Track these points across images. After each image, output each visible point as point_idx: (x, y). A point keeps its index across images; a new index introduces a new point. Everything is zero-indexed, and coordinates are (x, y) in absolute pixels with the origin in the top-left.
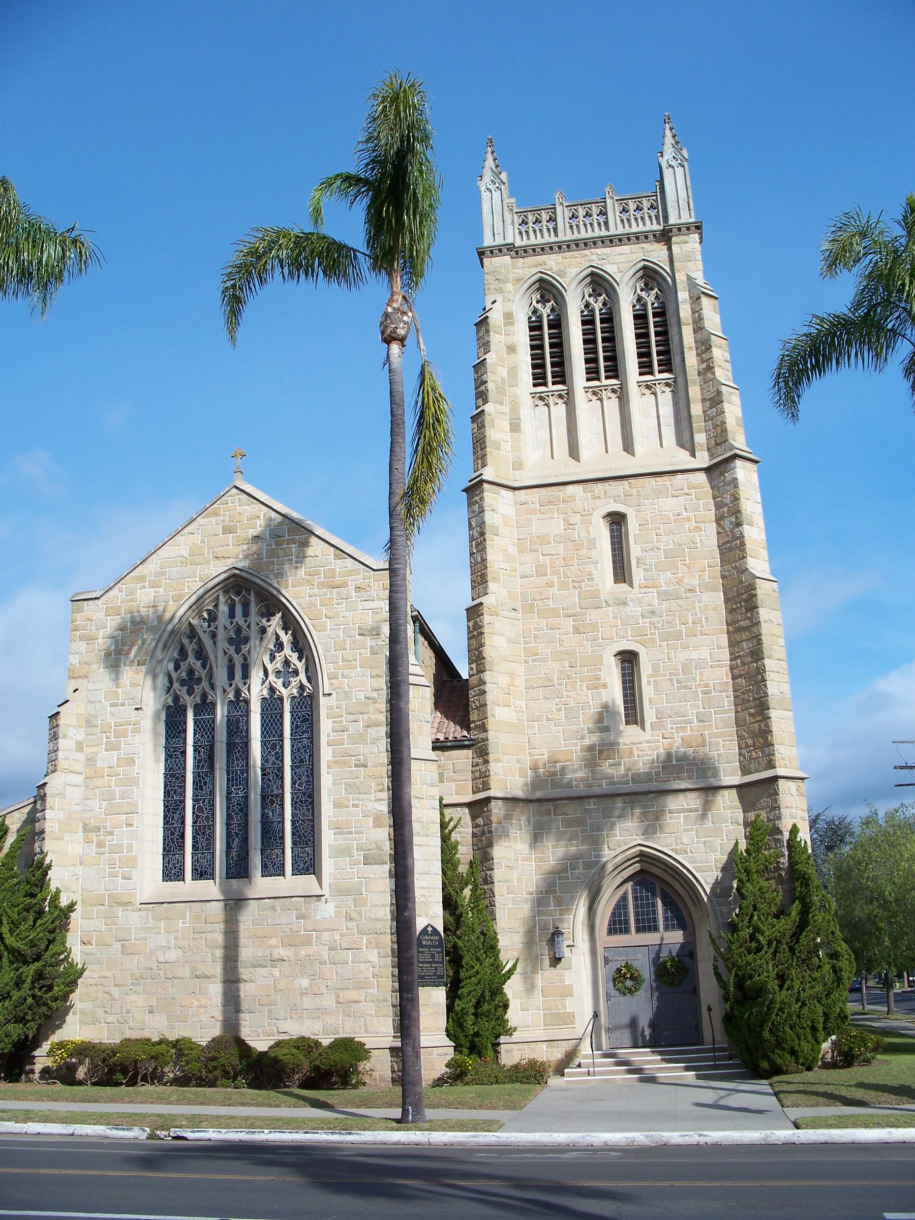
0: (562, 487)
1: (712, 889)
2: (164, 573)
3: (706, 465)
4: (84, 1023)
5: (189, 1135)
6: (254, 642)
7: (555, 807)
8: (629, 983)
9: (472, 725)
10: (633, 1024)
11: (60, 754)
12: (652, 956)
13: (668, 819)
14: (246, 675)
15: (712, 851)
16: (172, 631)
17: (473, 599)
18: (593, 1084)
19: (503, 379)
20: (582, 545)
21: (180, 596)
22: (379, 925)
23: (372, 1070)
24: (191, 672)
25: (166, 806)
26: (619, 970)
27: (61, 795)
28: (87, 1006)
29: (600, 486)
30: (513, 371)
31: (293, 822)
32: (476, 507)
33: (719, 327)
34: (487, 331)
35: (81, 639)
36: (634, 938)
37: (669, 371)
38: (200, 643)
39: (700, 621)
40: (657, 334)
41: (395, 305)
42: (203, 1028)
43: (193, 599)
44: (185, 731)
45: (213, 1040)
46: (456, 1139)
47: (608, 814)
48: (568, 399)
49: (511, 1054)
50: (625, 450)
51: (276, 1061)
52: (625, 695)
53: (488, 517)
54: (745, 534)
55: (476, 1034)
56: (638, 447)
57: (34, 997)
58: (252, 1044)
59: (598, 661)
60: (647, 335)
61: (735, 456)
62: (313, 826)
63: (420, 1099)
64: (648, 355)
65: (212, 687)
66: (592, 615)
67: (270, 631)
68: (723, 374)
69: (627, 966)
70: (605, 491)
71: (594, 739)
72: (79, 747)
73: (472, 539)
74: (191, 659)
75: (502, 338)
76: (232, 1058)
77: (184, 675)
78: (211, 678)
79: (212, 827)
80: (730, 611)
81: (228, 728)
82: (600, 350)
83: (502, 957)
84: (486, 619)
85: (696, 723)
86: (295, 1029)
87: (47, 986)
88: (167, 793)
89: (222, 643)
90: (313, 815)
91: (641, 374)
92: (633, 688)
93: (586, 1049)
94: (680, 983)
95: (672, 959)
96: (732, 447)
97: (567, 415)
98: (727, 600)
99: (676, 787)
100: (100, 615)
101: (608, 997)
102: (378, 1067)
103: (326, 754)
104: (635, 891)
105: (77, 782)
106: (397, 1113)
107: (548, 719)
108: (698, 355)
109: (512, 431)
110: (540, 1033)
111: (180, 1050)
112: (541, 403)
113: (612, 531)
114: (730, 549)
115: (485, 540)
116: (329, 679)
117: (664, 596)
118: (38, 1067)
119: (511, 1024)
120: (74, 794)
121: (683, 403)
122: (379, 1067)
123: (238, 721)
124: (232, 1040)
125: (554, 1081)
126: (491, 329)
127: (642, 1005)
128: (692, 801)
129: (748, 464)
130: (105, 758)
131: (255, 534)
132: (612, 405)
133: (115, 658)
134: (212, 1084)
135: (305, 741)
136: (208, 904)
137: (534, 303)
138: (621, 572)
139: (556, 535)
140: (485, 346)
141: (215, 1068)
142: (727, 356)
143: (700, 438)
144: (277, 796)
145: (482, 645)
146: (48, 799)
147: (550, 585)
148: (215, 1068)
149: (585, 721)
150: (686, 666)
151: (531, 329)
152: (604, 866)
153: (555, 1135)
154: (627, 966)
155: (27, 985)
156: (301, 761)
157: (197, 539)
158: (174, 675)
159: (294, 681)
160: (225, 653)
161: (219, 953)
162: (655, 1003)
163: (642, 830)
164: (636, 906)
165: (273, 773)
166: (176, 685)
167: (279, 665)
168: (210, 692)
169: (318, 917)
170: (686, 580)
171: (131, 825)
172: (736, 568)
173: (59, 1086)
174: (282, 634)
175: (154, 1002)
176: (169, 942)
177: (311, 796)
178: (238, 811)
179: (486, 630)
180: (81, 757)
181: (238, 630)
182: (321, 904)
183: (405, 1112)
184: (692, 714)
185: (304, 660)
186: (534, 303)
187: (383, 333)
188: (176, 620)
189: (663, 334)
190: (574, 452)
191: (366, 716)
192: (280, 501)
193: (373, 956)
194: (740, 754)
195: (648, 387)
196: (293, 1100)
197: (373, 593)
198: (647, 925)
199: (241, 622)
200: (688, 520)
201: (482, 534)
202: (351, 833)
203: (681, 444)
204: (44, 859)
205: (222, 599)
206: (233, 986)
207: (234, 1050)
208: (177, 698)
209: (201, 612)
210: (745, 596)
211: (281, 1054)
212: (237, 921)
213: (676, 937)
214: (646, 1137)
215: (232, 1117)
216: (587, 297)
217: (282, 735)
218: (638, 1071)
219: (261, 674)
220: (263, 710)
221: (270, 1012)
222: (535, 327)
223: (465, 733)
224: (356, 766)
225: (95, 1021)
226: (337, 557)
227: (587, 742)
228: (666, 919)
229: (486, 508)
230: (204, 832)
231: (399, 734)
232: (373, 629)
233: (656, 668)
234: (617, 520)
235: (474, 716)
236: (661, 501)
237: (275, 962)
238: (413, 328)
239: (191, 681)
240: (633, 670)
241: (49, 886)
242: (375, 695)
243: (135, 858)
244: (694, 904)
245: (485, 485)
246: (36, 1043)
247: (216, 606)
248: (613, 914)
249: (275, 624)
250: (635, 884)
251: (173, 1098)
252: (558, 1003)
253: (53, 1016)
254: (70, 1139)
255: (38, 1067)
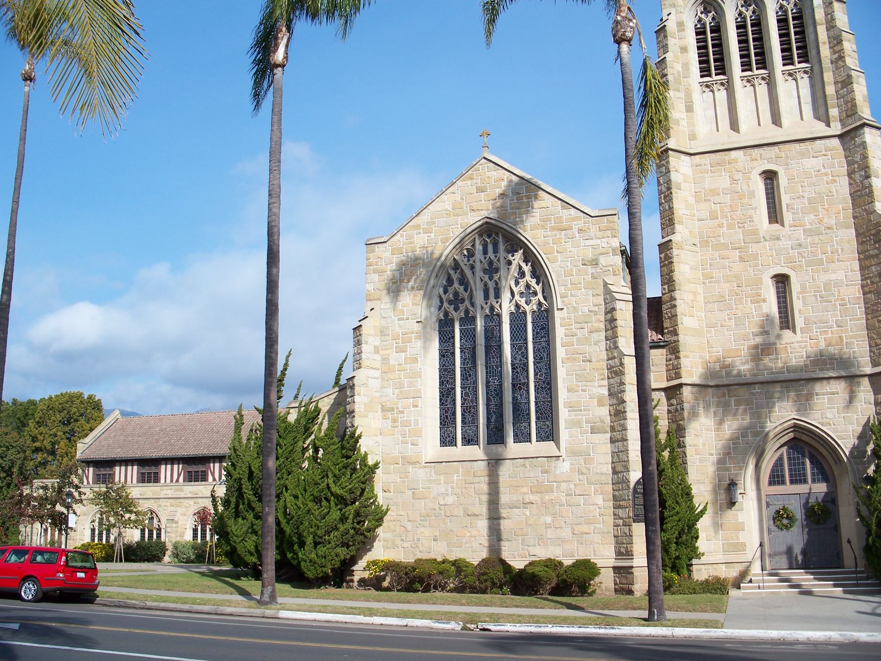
0: (727, 153)
1: (851, 452)
2: (434, 223)
3: (839, 133)
4: (387, 547)
5: (492, 627)
6: (502, 272)
7: (729, 391)
8: (785, 521)
9: (666, 331)
10: (789, 551)
11: (363, 356)
12: (803, 501)
13: (816, 399)
14: (498, 296)
15: (850, 424)
16: (442, 265)
17: (663, 237)
18: (764, 595)
19: (679, 72)
20: (744, 195)
21: (447, 239)
22: (603, 478)
23: (601, 583)
24: (456, 294)
25: (441, 392)
26: (778, 512)
27: (365, 385)
28: (388, 535)
29: (757, 151)
30: (686, 66)
31: (536, 403)
32: (663, 169)
33: (847, 25)
34: (665, 37)
35: (374, 272)
36: (788, 488)
37: (807, 61)
38: (462, 273)
39: (837, 251)
40: (796, 33)
41: (623, 14)
42: (474, 552)
43: (457, 240)
44: (453, 337)
45: (483, 560)
46: (693, 634)
47: (770, 397)
48: (729, 86)
49: (701, 572)
50: (773, 123)
51: (534, 576)
52: (779, 308)
53: (674, 176)
54: (873, 184)
55: (678, 558)
56: (785, 121)
57: (354, 529)
58: (511, 563)
59: (759, 282)
60: (788, 35)
61: (864, 125)
62: (551, 406)
63: (662, 604)
64: (789, 50)
65: (473, 305)
66: (753, 248)
67: (515, 263)
68: (851, 61)
69: (784, 509)
70: (761, 155)
71: (759, 340)
72: (377, 350)
73: (660, 192)
74: (456, 285)
75: (676, 41)
76: (498, 574)
77: (523, 289)
78: (471, 299)
79: (476, 407)
80: (860, 243)
81: (486, 334)
82: (752, 47)
83: (696, 501)
84: (675, 252)
85: (835, 328)
86: (542, 553)
87: (360, 518)
88: (442, 383)
89: (479, 273)
90: (551, 397)
91: (784, 65)
92: (786, 302)
93: (756, 568)
94: (825, 522)
95: (819, 504)
96: (861, 118)
97: (728, 98)
98: (858, 235)
99: (821, 376)
100: (388, 254)
101: (770, 531)
102: (604, 580)
103: (561, 353)
104: (788, 454)
105: (376, 376)
106: (645, 614)
107: (722, 326)
108: (830, 48)
109: (687, 111)
110: (720, 557)
111: (458, 567)
112: (707, 90)
113: (766, 184)
114: (861, 196)
115: (671, 193)
116: (561, 298)
117: (808, 233)
118: (356, 578)
119: (701, 550)
120: (375, 384)
121: (818, 86)
122: (606, 581)
123: (493, 329)
124: (495, 560)
125: (733, 592)
126: (668, 35)
127: (796, 538)
128: (840, 387)
129: (874, 131)
130: (396, 358)
131: (501, 192)
132: (762, 89)
133: (395, 288)
134: (484, 592)
135: (544, 344)
136: (475, 463)
137: (699, 14)
138: (774, 214)
139: (724, 189)
140: (665, 48)
141: (486, 581)
142: (854, 47)
143: (834, 112)
144: (524, 384)
145: (672, 271)
146: (357, 388)
147: (721, 226)
148: (486, 581)
149: (752, 327)
150: (827, 285)
151: (697, 34)
152: (767, 434)
153: (769, 632)
154: (784, 509)
155: (350, 521)
156: (541, 358)
157: (458, 197)
158: (444, 297)
159: (534, 300)
160: (482, 280)
161: (485, 498)
162: (806, 537)
163: (796, 408)
164: (790, 465)
165: (520, 367)
166: (446, 305)
167: (522, 287)
168: (471, 308)
169: (558, 472)
170: (826, 220)
171: (416, 406)
172: (865, 210)
173: (373, 592)
174: (523, 265)
175: (437, 533)
176: (447, 490)
177: (549, 384)
178: (495, 394)
179: (675, 260)
180: (378, 357)
181: (491, 263)
182: (560, 462)
183: (651, 613)
184: (832, 321)
185: (541, 284)
186: (699, 14)
187: (614, 36)
188: (443, 258)
189: (801, 32)
190: (734, 125)
191: (589, 325)
192: (518, 168)
193: (599, 500)
194: (871, 351)
195: (790, 75)
196: (552, 604)
197: (592, 234)
198: (798, 478)
199: (493, 257)
200: (826, 174)
201: (669, 189)
202: (581, 410)
203: (817, 117)
204: (355, 431)
205: (477, 242)
206: (495, 522)
207: (500, 568)
208: (446, 314)
209: (462, 250)
210: (873, 232)
211: (536, 570)
212: (497, 475)
213: (821, 488)
214: (841, 635)
215: (520, 616)
216: (740, 7)
217: (526, 339)
218: (798, 586)
219: (509, 295)
220: (511, 321)
221: (523, 540)
222: (700, 32)
223: (660, 337)
224: (583, 361)
225: (395, 546)
226: (563, 208)
227: (752, 343)
228: (813, 474)
229: (671, 169)
230: (470, 412)
231: (641, 335)
232: (593, 260)
233: (803, 287)
234: (770, 177)
235: (667, 324)
236: (805, 161)
237: (526, 504)
238: (637, 33)
239: (456, 301)
240: (785, 288)
241: (359, 450)
242: (596, 309)
243: (420, 431)
244: (836, 463)
245: (670, 152)
246: (353, 560)
247: (473, 246)
248: (773, 471)
249: (517, 258)
250: (789, 448)
251: (464, 601)
252: (734, 537)
253: (365, 541)
254: (405, 629)
255: (356, 578)
